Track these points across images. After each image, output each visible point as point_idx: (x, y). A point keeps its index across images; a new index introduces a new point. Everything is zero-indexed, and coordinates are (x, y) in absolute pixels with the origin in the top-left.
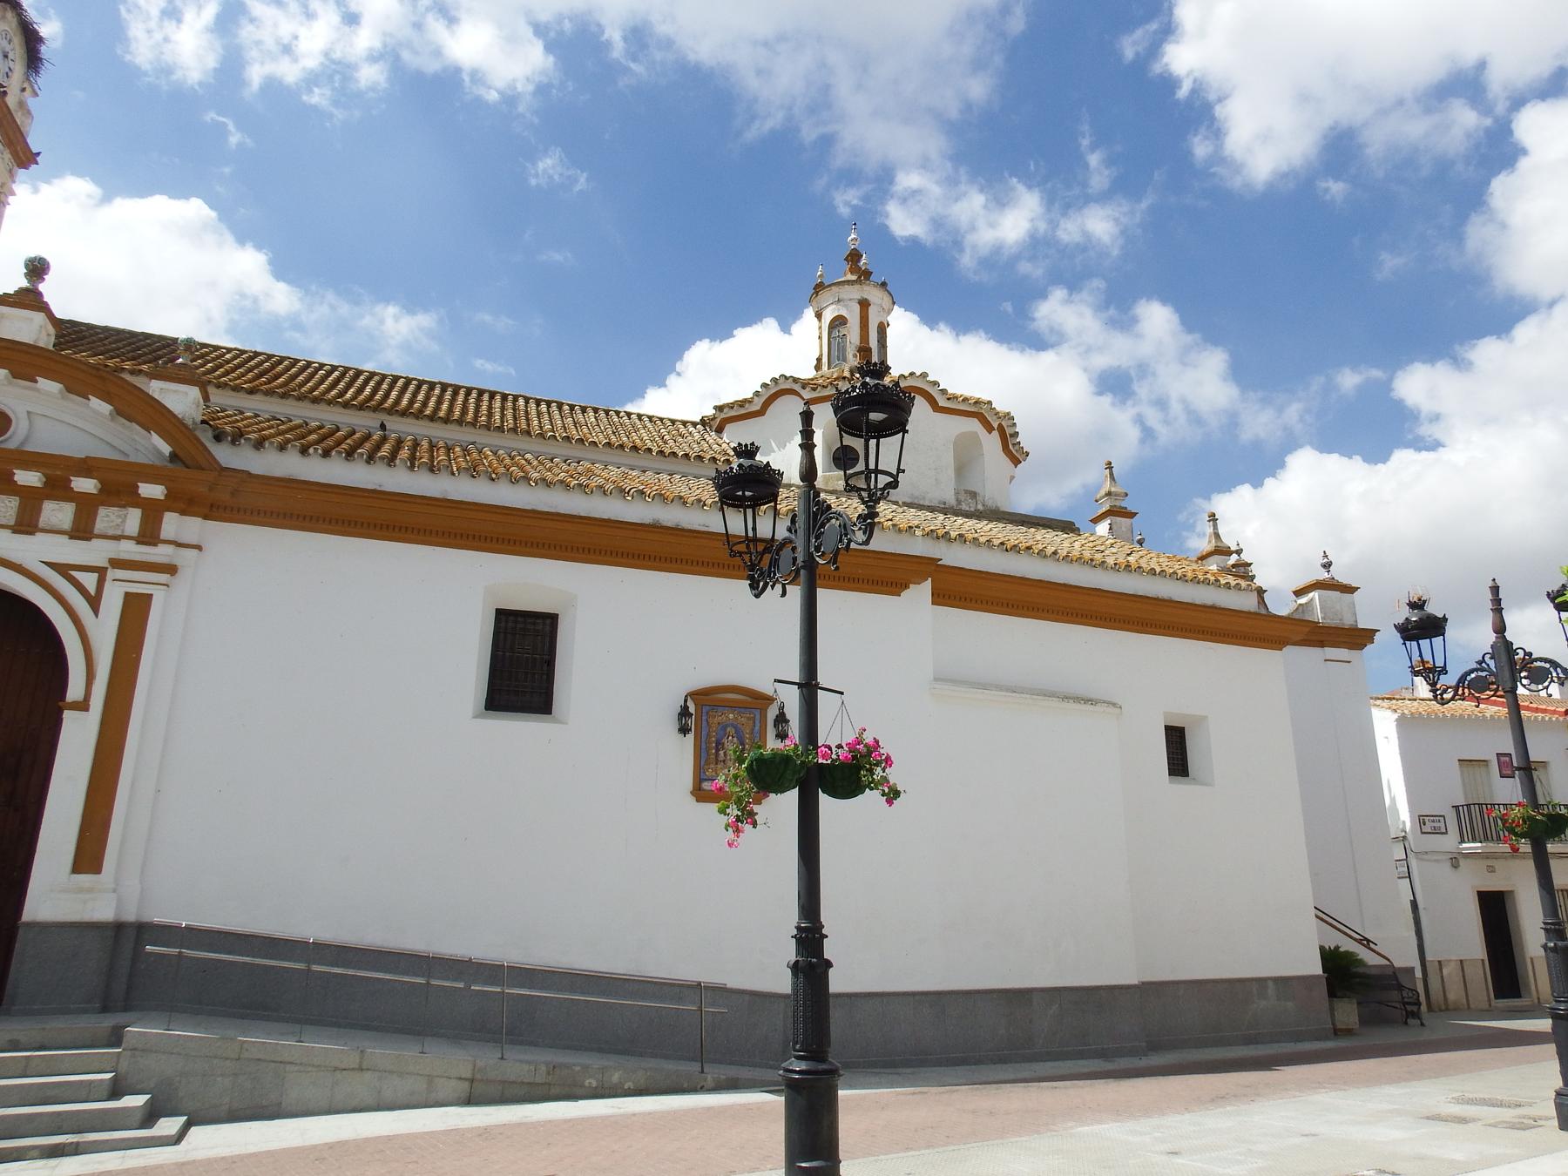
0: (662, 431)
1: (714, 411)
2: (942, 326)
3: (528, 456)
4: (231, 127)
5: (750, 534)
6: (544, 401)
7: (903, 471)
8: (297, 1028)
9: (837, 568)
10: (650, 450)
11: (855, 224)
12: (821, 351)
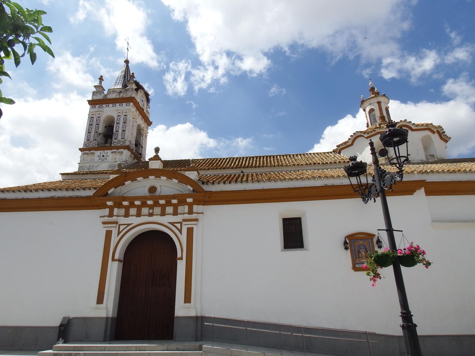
1: (337, 147)
2: (409, 102)
3: (284, 172)
4: (193, 104)
6: (285, 155)
7: (409, 155)
9: (392, 190)
10: (319, 163)
11: (370, 79)
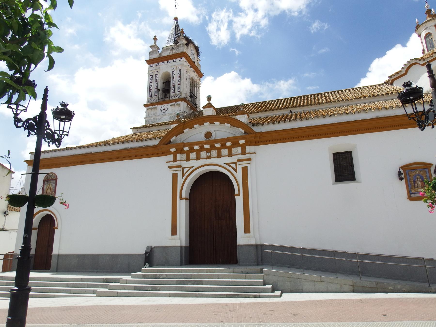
0: (372, 89)
1: (389, 78)
3: (332, 108)
4: (236, 50)
5: (415, 112)
6: (333, 92)
8: (303, 270)
10: (370, 96)
12: (423, 47)
